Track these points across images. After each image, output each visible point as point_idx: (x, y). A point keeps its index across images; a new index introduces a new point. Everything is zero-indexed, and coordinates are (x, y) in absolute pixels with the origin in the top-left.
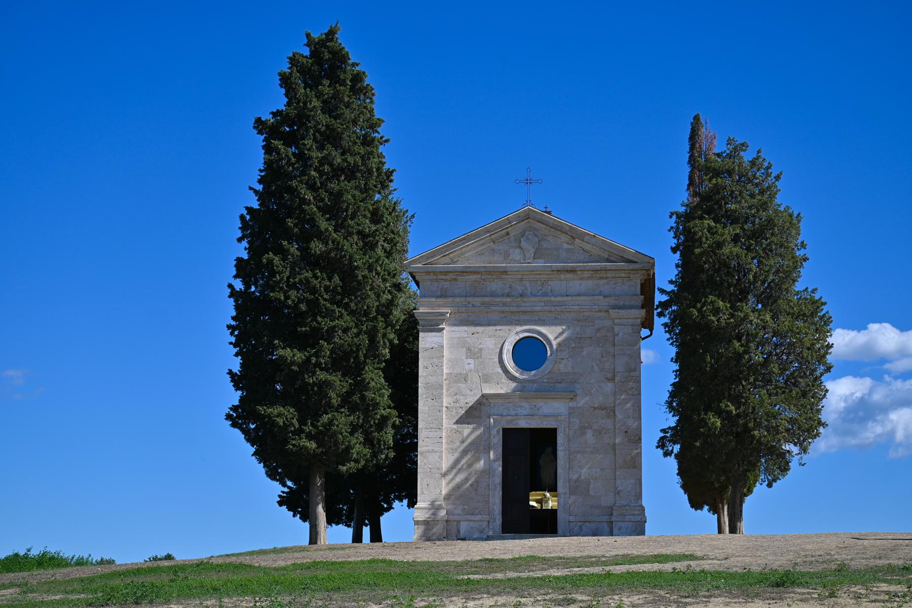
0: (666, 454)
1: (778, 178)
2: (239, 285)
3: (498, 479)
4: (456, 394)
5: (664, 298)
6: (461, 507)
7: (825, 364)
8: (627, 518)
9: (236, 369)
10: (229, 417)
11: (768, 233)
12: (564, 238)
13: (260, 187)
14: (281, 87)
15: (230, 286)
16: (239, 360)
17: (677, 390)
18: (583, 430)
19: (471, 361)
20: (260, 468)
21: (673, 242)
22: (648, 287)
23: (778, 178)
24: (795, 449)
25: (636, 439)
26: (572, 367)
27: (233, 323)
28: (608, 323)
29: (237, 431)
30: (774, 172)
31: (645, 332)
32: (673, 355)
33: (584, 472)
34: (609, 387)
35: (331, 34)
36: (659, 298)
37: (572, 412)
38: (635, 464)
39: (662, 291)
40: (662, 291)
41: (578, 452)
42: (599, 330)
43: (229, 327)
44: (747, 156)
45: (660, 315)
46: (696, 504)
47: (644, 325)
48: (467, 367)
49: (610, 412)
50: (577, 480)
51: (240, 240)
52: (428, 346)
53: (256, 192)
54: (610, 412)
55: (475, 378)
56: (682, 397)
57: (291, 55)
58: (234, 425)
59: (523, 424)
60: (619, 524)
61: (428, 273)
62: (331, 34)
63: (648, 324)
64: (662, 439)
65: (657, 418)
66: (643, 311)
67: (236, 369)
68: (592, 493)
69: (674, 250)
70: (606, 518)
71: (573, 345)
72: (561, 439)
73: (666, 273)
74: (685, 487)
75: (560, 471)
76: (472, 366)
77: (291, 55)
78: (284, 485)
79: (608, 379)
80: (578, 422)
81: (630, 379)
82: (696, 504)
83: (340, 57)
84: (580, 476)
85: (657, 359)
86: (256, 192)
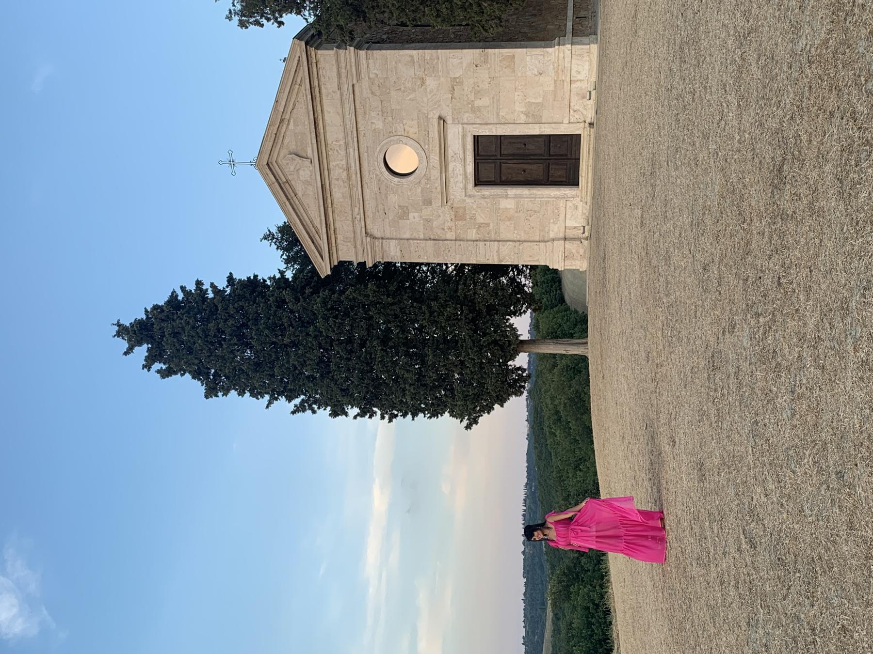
4: (443, 229)
6: (551, 225)
8: (568, 65)
13: (267, 397)
15: (355, 417)
19: (411, 215)
26: (413, 120)
32: (198, 387)
34: (431, 83)
41: (498, 115)
42: (372, 93)
43: (390, 421)
48: (417, 219)
52: (399, 254)
55: (427, 212)
57: (146, 370)
60: (574, 73)
68: (540, 100)
71: (390, 118)
76: (416, 215)
77: (146, 370)
78: (525, 312)
79: (423, 82)
80: (467, 115)
84: (522, 112)
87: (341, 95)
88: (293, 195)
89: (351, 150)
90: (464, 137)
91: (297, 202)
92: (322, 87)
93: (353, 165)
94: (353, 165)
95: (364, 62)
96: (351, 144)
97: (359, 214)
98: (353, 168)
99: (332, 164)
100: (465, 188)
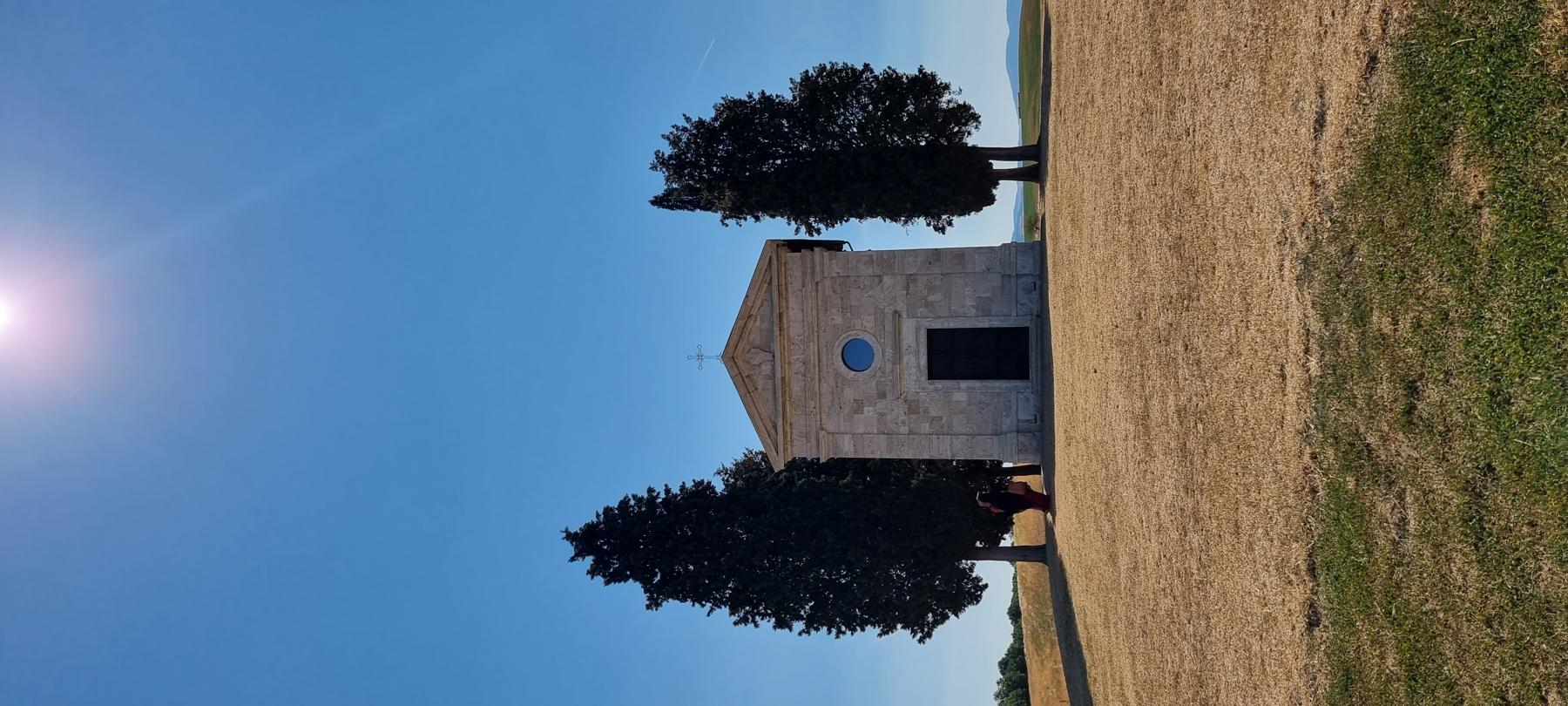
0: (950, 224)
1: (688, 119)
2: (799, 625)
3: (976, 384)
5: (803, 229)
7: (863, 72)
9: (878, 630)
10: (921, 640)
11: (744, 121)
12: (750, 325)
14: (614, 577)
16: (869, 628)
17: (893, 214)
18: (928, 304)
20: (970, 609)
21: (750, 219)
22: (794, 246)
23: (688, 119)
24: (946, 97)
25: (937, 254)
27: (834, 631)
28: (828, 283)
29: (935, 632)
30: (682, 123)
31: (846, 247)
33: (969, 302)
34: (887, 280)
35: (570, 537)
36: (803, 235)
37: (911, 315)
38: (960, 255)
39: (797, 230)
40: (797, 230)
44: (668, 150)
45: (818, 231)
46: (990, 200)
47: (840, 249)
49: (911, 278)
50: (977, 308)
51: (757, 626)
53: (712, 610)
54: (911, 278)
56: (898, 209)
58: (929, 635)
59: (924, 361)
61: (785, 449)
62: (570, 537)
63: (836, 246)
64: (936, 229)
65: (917, 235)
66: (817, 249)
67: (878, 630)
69: (757, 219)
70: (1013, 280)
72: (937, 325)
73: (781, 228)
74: (979, 209)
75: (968, 325)
81: (886, 261)
82: (990, 200)
83: (590, 529)
85: (868, 235)
86: (712, 610)
90: (918, 330)
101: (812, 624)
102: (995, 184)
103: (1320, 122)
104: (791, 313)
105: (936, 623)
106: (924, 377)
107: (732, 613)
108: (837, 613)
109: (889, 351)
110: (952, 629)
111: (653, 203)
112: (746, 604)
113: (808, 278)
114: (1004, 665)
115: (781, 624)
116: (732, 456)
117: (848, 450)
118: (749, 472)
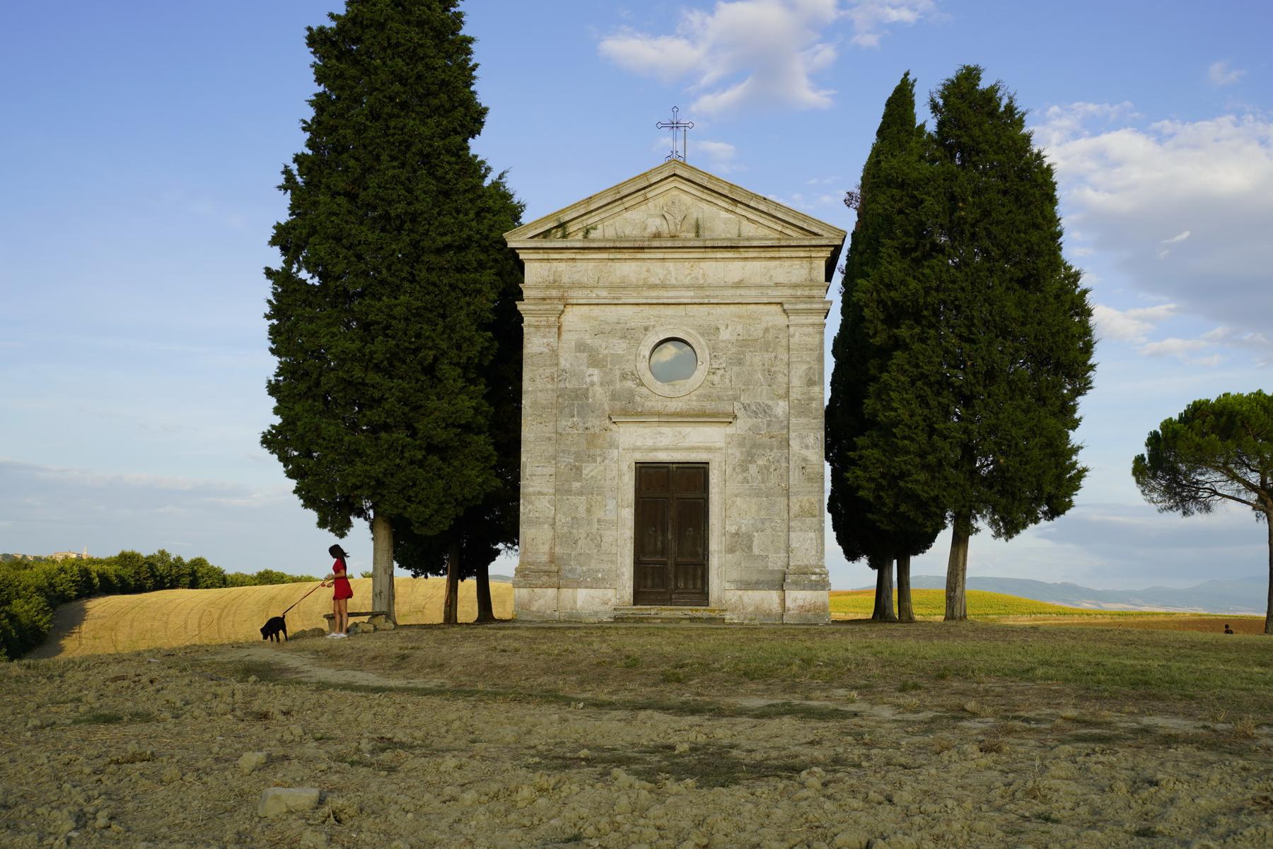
2: (276, 260)
19: (596, 371)
59: (663, 457)
68: (756, 551)
87: (768, 287)
88: (627, 205)
89: (692, 293)
90: (709, 449)
91: (617, 210)
92: (777, 263)
93: (671, 294)
94: (671, 294)
95: (811, 321)
96: (701, 293)
97: (598, 297)
98: (665, 294)
99: (670, 265)
100: (635, 449)
101: (280, 278)
102: (872, 565)
103: (715, 768)
104: (738, 265)
105: (284, 459)
106: (641, 457)
107: (298, 159)
108: (291, 315)
109: (673, 406)
110: (273, 481)
111: (905, 81)
112: (312, 181)
113: (789, 292)
114: (199, 562)
115: (284, 238)
116: (518, 188)
117: (534, 344)
118: (504, 209)
